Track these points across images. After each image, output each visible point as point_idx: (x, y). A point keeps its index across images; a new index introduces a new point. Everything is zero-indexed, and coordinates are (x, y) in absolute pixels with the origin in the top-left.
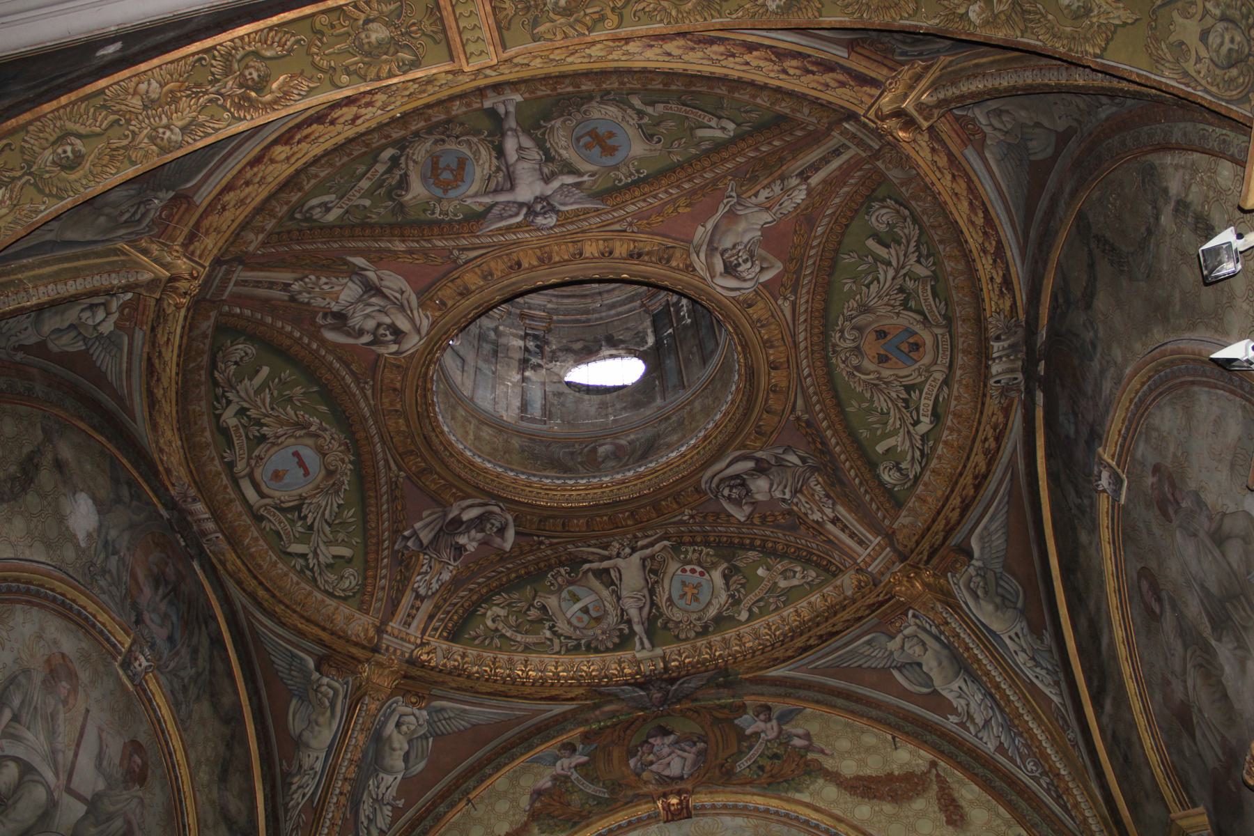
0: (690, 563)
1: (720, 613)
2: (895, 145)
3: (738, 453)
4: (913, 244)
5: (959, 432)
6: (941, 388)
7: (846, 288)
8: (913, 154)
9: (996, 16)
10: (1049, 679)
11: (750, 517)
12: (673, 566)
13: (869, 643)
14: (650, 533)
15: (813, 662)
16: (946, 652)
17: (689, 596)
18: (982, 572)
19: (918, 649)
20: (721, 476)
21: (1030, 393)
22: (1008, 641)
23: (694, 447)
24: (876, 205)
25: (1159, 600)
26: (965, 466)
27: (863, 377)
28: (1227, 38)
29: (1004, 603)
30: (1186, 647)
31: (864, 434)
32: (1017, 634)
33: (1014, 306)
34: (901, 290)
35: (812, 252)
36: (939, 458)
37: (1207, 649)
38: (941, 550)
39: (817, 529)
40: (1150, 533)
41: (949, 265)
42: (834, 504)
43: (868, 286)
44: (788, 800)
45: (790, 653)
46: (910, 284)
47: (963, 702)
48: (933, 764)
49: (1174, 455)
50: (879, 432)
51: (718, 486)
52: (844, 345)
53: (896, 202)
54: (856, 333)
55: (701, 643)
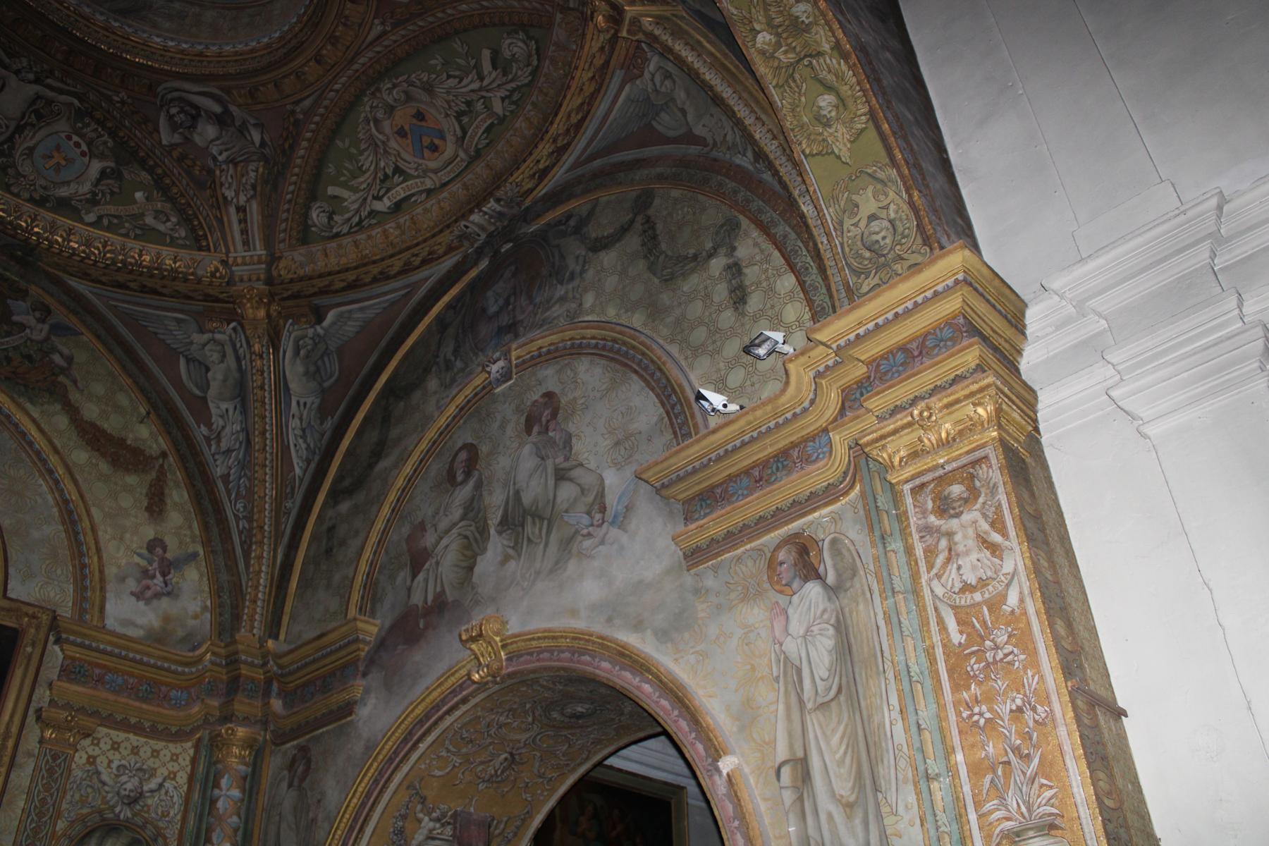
0: (82, 136)
1: (70, 199)
2: (587, 19)
3: (219, 92)
4: (513, 85)
5: (403, 233)
6: (421, 192)
7: (433, 62)
8: (589, 37)
9: (772, 57)
10: (304, 454)
11: (173, 146)
12: (62, 126)
13: (179, 321)
14: (69, 81)
15: (117, 300)
16: (236, 375)
17: (53, 161)
18: (317, 340)
19: (216, 357)
20: (184, 94)
21: (479, 253)
22: (294, 404)
23: (182, 52)
24: (521, 35)
25: (468, 474)
26: (383, 259)
27: (374, 130)
28: (883, 234)
29: (314, 373)
30: (463, 518)
31: (331, 169)
32: (305, 404)
33: (531, 191)
34: (469, 103)
35: (440, 15)
36: (369, 237)
37: (483, 531)
38: (300, 299)
39: (220, 204)
40: (502, 427)
41: (520, 123)
42: (252, 197)
43: (449, 77)
44: (19, 405)
45: (104, 279)
46: (479, 106)
47: (221, 423)
48: (164, 455)
49: (575, 399)
50: (342, 179)
51: (172, 100)
52: (385, 97)
53: (537, 50)
54: (403, 97)
55: (28, 208)
